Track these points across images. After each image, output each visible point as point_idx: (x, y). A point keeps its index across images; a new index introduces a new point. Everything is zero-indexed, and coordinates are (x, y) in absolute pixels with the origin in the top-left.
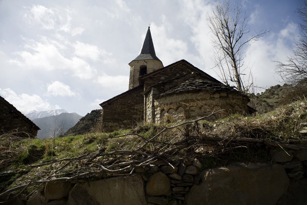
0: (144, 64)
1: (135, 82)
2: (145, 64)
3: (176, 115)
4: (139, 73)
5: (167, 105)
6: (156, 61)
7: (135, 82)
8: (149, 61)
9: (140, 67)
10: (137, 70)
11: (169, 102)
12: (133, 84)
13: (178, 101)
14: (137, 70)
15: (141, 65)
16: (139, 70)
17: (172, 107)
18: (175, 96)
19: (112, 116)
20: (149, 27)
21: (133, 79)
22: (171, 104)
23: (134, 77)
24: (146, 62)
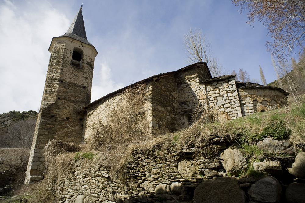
0: (80, 48)
1: (66, 64)
2: (81, 48)
3: (270, 107)
4: (72, 55)
5: (260, 96)
6: (94, 50)
7: (66, 64)
8: (87, 46)
9: (74, 49)
10: (70, 51)
11: (263, 94)
12: (62, 66)
13: (272, 95)
14: (70, 51)
15: (76, 47)
16: (72, 52)
17: (266, 99)
18: (268, 91)
19: (159, 98)
20: (81, 9)
21: (63, 60)
22: (264, 96)
23: (64, 57)
24: (83, 46)
